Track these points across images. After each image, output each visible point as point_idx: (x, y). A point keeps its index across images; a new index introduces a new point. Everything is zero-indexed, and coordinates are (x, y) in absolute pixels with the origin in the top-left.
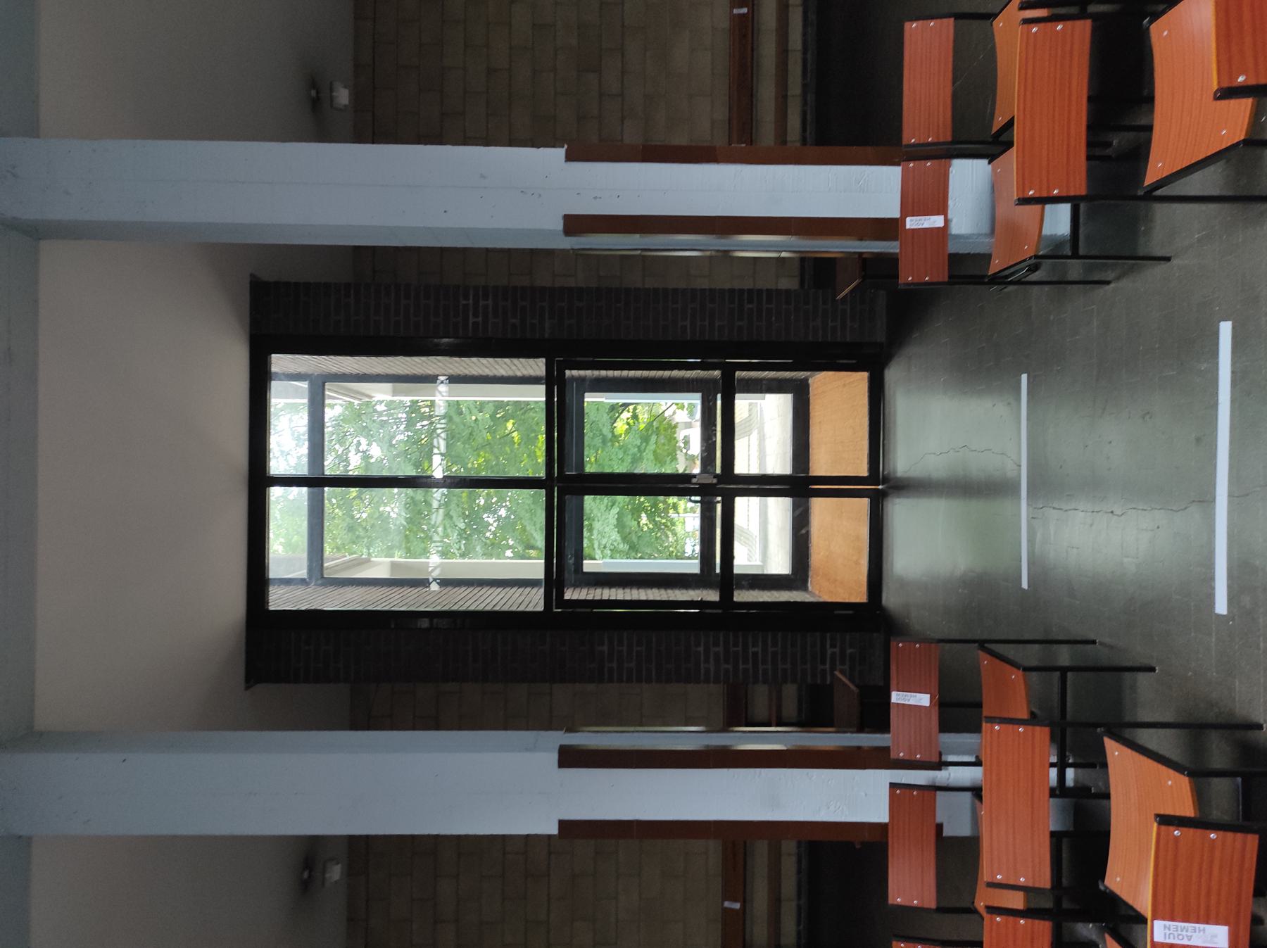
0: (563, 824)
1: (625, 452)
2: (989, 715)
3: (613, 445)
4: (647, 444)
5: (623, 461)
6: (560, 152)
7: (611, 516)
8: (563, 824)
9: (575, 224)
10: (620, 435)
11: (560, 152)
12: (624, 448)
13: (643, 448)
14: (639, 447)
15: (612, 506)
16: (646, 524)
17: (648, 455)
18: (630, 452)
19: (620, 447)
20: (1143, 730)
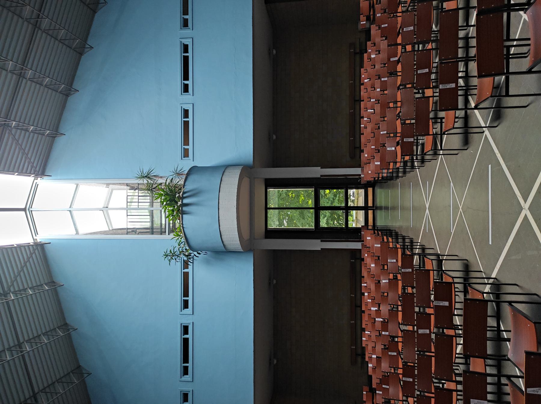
0: (321, 249)
1: (329, 200)
2: (358, 212)
3: (325, 198)
4: (336, 197)
5: (328, 203)
6: (320, 168)
7: (324, 220)
8: (321, 249)
9: (321, 176)
10: (327, 194)
11: (320, 168)
12: (328, 199)
13: (334, 198)
14: (333, 198)
15: (325, 217)
16: (336, 224)
17: (336, 201)
18: (331, 200)
19: (327, 198)
20: (460, 314)
